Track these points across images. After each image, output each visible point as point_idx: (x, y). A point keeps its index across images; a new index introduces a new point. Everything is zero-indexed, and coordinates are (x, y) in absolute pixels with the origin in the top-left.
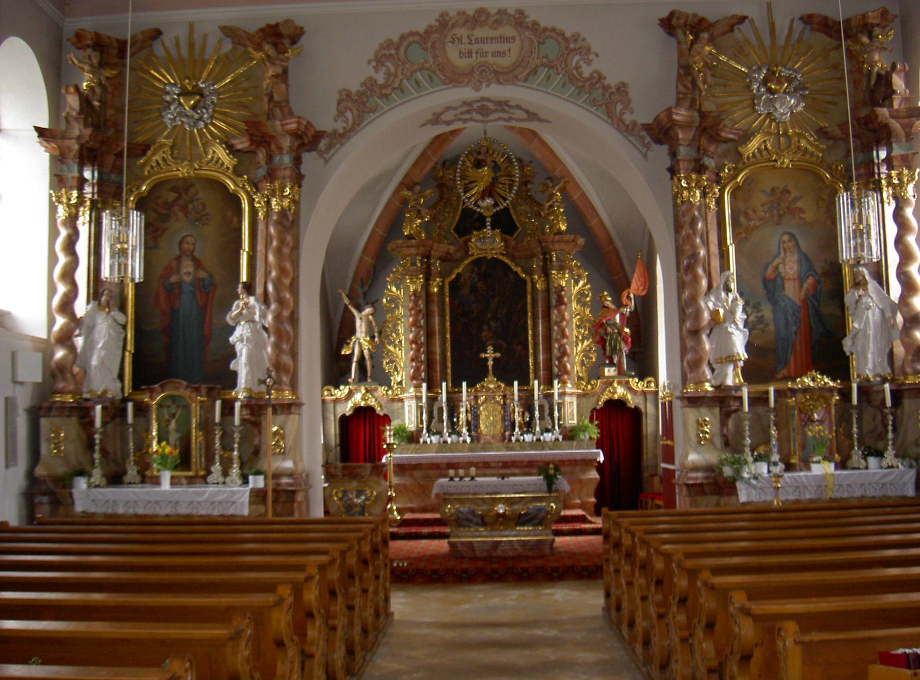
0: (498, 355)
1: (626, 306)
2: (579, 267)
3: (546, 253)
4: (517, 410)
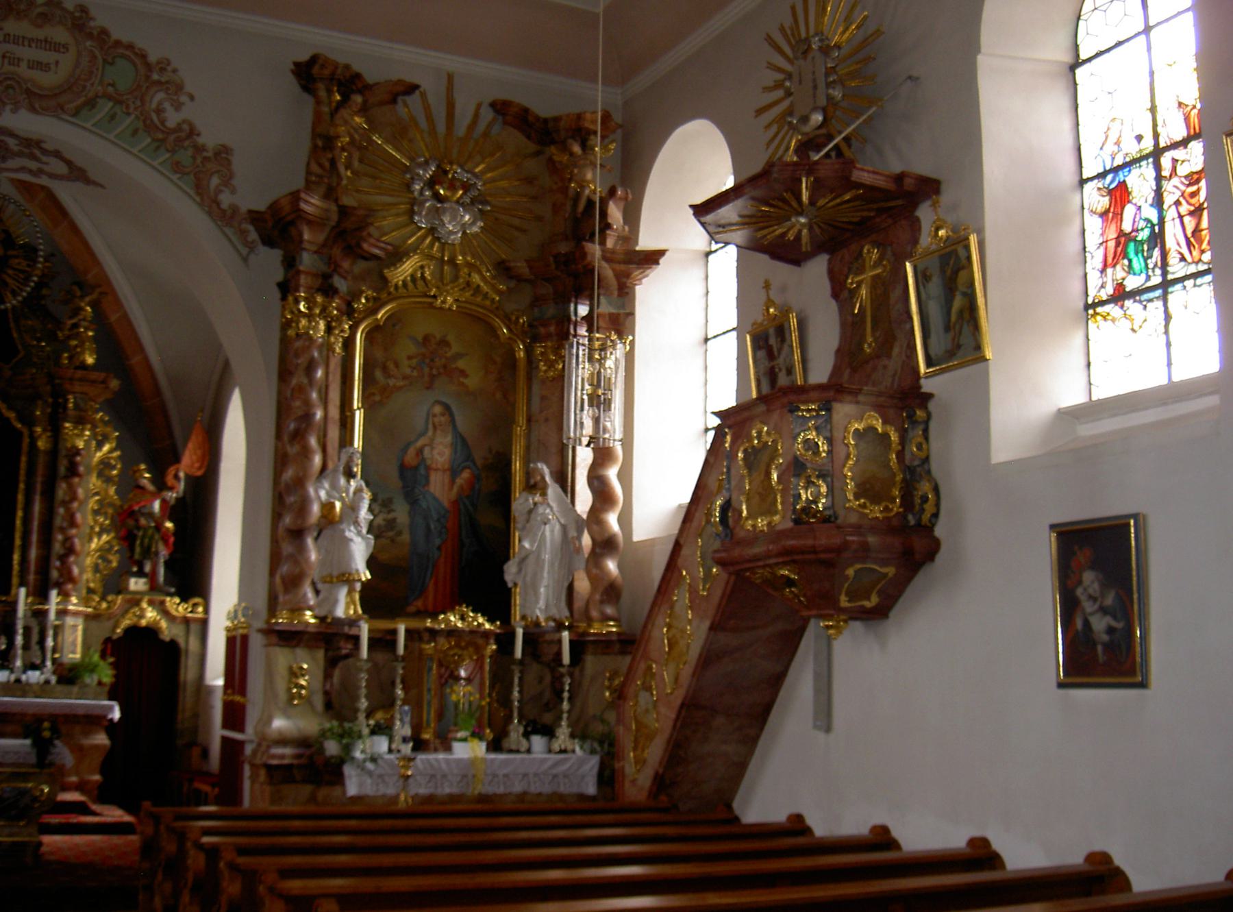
1: (171, 489)
2: (106, 423)
3: (59, 396)
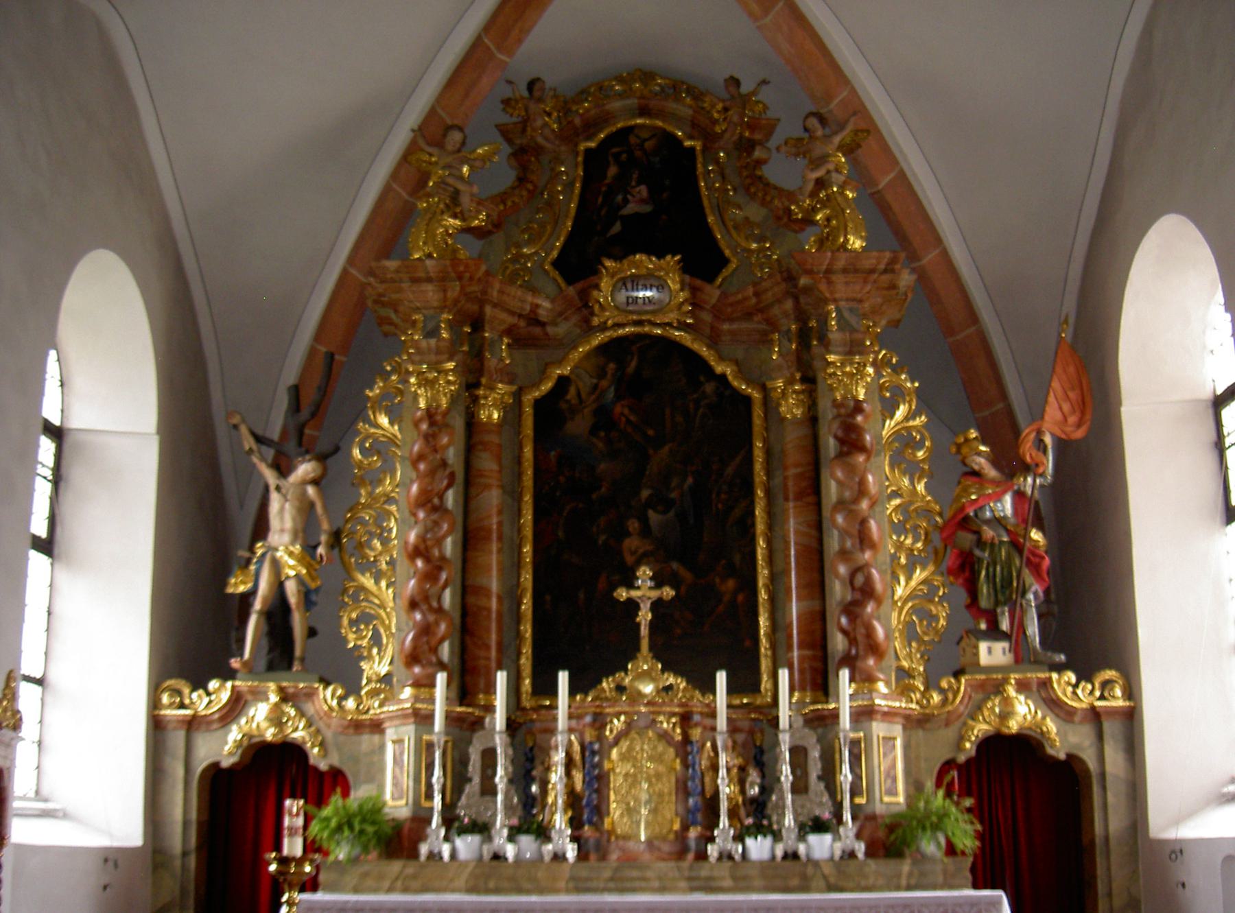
0: (668, 592)
4: (723, 759)
